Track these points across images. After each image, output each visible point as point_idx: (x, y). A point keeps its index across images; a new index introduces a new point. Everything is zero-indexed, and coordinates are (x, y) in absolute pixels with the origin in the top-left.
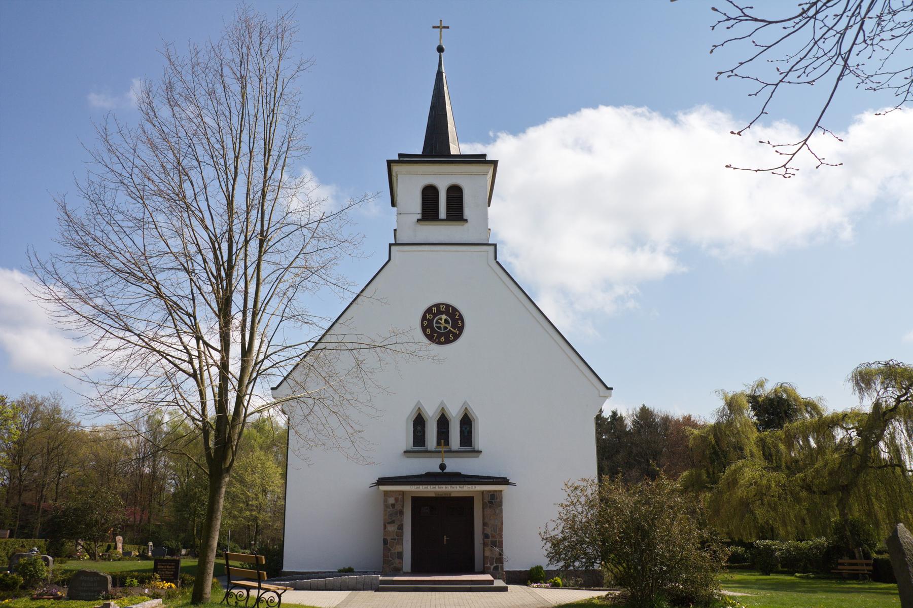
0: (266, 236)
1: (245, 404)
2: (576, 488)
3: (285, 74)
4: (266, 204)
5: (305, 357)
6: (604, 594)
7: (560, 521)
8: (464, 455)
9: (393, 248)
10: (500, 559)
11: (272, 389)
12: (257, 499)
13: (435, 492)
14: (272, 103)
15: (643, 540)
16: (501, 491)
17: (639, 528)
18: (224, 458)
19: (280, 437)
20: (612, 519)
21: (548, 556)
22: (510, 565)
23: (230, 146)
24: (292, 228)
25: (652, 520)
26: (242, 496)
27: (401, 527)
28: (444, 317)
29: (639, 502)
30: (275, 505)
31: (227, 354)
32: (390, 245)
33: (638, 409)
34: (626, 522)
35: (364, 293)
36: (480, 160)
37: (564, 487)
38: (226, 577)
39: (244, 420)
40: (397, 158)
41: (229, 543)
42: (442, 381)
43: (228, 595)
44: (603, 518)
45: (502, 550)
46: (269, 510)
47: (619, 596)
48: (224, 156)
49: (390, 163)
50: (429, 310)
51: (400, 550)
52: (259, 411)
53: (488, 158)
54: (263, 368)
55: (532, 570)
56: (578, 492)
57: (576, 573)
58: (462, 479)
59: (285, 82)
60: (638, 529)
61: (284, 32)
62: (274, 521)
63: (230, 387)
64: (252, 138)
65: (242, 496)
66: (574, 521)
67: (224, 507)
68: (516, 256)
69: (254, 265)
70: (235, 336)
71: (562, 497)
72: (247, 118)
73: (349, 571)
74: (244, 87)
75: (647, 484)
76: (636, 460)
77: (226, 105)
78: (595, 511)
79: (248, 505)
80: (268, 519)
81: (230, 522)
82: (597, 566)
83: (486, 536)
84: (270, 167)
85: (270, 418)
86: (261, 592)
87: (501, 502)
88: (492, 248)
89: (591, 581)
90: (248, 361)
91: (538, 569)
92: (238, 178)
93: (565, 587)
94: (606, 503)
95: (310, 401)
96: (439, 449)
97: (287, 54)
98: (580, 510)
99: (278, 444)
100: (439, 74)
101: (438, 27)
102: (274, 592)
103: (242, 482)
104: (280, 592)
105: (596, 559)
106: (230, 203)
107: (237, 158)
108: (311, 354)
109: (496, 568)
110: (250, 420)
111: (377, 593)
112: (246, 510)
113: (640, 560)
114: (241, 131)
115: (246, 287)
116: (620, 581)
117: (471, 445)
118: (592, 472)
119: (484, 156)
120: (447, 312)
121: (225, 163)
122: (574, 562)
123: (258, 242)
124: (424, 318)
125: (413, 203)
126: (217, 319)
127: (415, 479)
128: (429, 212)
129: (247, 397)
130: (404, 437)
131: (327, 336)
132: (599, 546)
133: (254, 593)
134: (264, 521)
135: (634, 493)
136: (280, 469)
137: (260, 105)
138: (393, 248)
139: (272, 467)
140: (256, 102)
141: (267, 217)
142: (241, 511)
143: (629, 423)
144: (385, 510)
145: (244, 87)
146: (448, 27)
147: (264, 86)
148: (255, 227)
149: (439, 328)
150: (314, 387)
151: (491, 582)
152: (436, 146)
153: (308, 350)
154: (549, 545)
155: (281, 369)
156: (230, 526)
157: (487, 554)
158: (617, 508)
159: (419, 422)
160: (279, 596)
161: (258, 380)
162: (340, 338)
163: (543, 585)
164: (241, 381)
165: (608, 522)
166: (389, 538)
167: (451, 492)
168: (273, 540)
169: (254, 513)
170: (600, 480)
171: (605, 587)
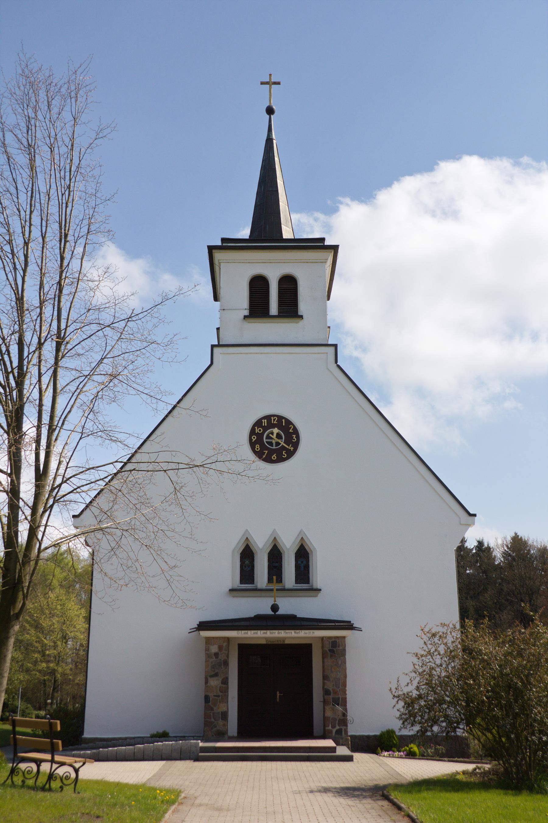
0: (64, 338)
1: (40, 537)
2: (434, 635)
3: (81, 142)
4: (63, 300)
5: (112, 479)
6: (470, 767)
7: (413, 674)
8: (300, 593)
9: (216, 350)
10: (344, 721)
11: (74, 516)
12: (55, 647)
13: (266, 638)
14: (67, 178)
15: (516, 701)
17: (510, 686)
18: (13, 601)
19: (86, 572)
20: (477, 674)
21: (400, 718)
22: (356, 728)
23: (19, 230)
24: (95, 327)
25: (527, 676)
26: (37, 645)
27: (225, 682)
28: (276, 431)
29: (510, 654)
30: (77, 654)
31: (18, 478)
32: (213, 346)
33: (509, 539)
34: (494, 678)
35: (182, 404)
36: (318, 244)
37: (420, 633)
38: (12, 748)
39: (38, 556)
40: (219, 243)
41: (20, 704)
42: (273, 506)
43: (13, 771)
44: (466, 673)
45: (346, 710)
46: (69, 660)
47: (489, 772)
48: (10, 242)
49: (211, 249)
50: (258, 423)
51: (225, 709)
52: (56, 545)
53: (327, 243)
54: (61, 493)
55: (383, 734)
56: (436, 640)
57: (435, 740)
58: (298, 623)
59: (82, 153)
60: (509, 687)
61: (78, 90)
62: (76, 674)
63: (21, 517)
64: (45, 220)
65: (37, 645)
66: (431, 675)
67: (13, 659)
68: (365, 350)
69: (51, 372)
70: (28, 456)
71: (418, 646)
72: (38, 196)
73: (164, 736)
74: (32, 160)
75: (520, 631)
76: (507, 600)
77: (10, 179)
78: (457, 663)
79: (44, 655)
80: (68, 672)
81: (21, 677)
82: (459, 732)
83: (326, 692)
84: (67, 255)
85: (69, 550)
86: (55, 766)
88: (332, 349)
89: (455, 751)
90: (43, 487)
91: (390, 733)
92: (29, 269)
93: (424, 756)
94: (470, 654)
95: (119, 533)
96: (271, 587)
97: (84, 118)
98: (438, 662)
99: (82, 581)
100: (269, 141)
101: (267, 83)
102: (71, 765)
103: (37, 626)
104: (77, 765)
105: (458, 723)
106: (20, 300)
107: (26, 244)
108: (119, 476)
109: (339, 732)
110: (44, 555)
111: (197, 764)
112: (41, 661)
113: (513, 726)
114: (31, 212)
115: (41, 399)
116: (490, 752)
117: (308, 582)
118: (453, 615)
119: (323, 240)
120: (279, 425)
121: (12, 251)
122: (432, 726)
123: (54, 344)
124: (252, 432)
125: (239, 297)
126: (6, 436)
127: (243, 623)
128: (258, 308)
129: (42, 529)
130: (229, 573)
131: (138, 456)
132: (463, 707)
133: (45, 767)
134: (63, 674)
135: (504, 643)
136: (83, 611)
137: (53, 180)
138: (216, 350)
139: (74, 609)
140: (48, 177)
141: (64, 315)
142: (35, 663)
143: (498, 555)
144: (207, 661)
145: (32, 160)
146: (279, 83)
147: (57, 157)
148: (50, 326)
149: (271, 444)
150: (123, 517)
151: (333, 750)
152: (266, 227)
153: (115, 471)
154: (401, 704)
155: (83, 494)
156: (21, 681)
157: (329, 714)
158: (483, 660)
159: (247, 555)
160: (77, 771)
161: (55, 506)
162: (153, 457)
163: (397, 754)
164: (34, 509)
165: (472, 677)
166: (211, 695)
168: (74, 697)
169: (52, 665)
170: (463, 626)
171: (472, 759)
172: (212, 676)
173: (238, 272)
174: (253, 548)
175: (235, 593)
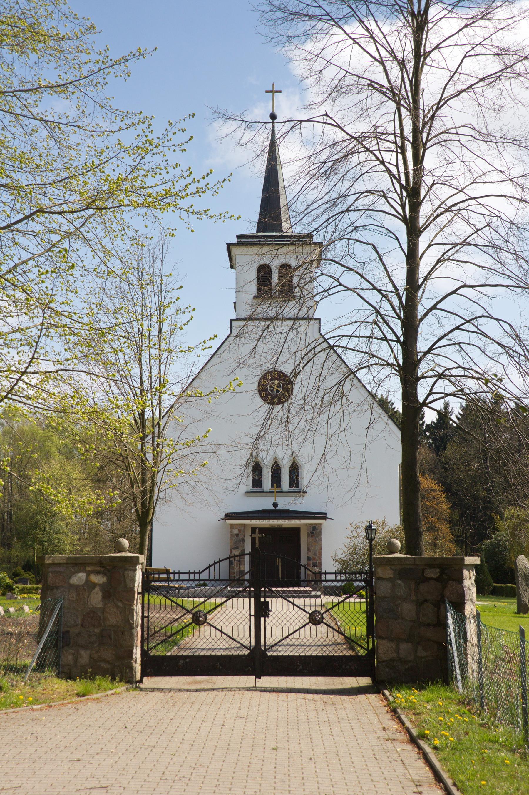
16: (321, 524)
32: (232, 320)
87: (321, 532)
88: (317, 321)
127: (254, 515)
144: (231, 539)
149: (272, 391)
167: (282, 525)
172: (234, 549)
173: (250, 260)
174: (262, 464)
175: (248, 495)
